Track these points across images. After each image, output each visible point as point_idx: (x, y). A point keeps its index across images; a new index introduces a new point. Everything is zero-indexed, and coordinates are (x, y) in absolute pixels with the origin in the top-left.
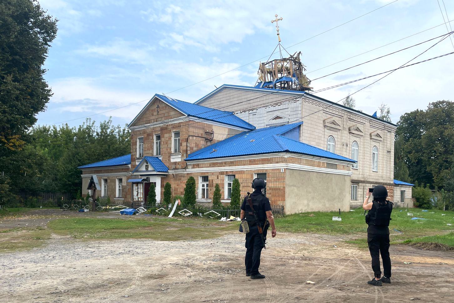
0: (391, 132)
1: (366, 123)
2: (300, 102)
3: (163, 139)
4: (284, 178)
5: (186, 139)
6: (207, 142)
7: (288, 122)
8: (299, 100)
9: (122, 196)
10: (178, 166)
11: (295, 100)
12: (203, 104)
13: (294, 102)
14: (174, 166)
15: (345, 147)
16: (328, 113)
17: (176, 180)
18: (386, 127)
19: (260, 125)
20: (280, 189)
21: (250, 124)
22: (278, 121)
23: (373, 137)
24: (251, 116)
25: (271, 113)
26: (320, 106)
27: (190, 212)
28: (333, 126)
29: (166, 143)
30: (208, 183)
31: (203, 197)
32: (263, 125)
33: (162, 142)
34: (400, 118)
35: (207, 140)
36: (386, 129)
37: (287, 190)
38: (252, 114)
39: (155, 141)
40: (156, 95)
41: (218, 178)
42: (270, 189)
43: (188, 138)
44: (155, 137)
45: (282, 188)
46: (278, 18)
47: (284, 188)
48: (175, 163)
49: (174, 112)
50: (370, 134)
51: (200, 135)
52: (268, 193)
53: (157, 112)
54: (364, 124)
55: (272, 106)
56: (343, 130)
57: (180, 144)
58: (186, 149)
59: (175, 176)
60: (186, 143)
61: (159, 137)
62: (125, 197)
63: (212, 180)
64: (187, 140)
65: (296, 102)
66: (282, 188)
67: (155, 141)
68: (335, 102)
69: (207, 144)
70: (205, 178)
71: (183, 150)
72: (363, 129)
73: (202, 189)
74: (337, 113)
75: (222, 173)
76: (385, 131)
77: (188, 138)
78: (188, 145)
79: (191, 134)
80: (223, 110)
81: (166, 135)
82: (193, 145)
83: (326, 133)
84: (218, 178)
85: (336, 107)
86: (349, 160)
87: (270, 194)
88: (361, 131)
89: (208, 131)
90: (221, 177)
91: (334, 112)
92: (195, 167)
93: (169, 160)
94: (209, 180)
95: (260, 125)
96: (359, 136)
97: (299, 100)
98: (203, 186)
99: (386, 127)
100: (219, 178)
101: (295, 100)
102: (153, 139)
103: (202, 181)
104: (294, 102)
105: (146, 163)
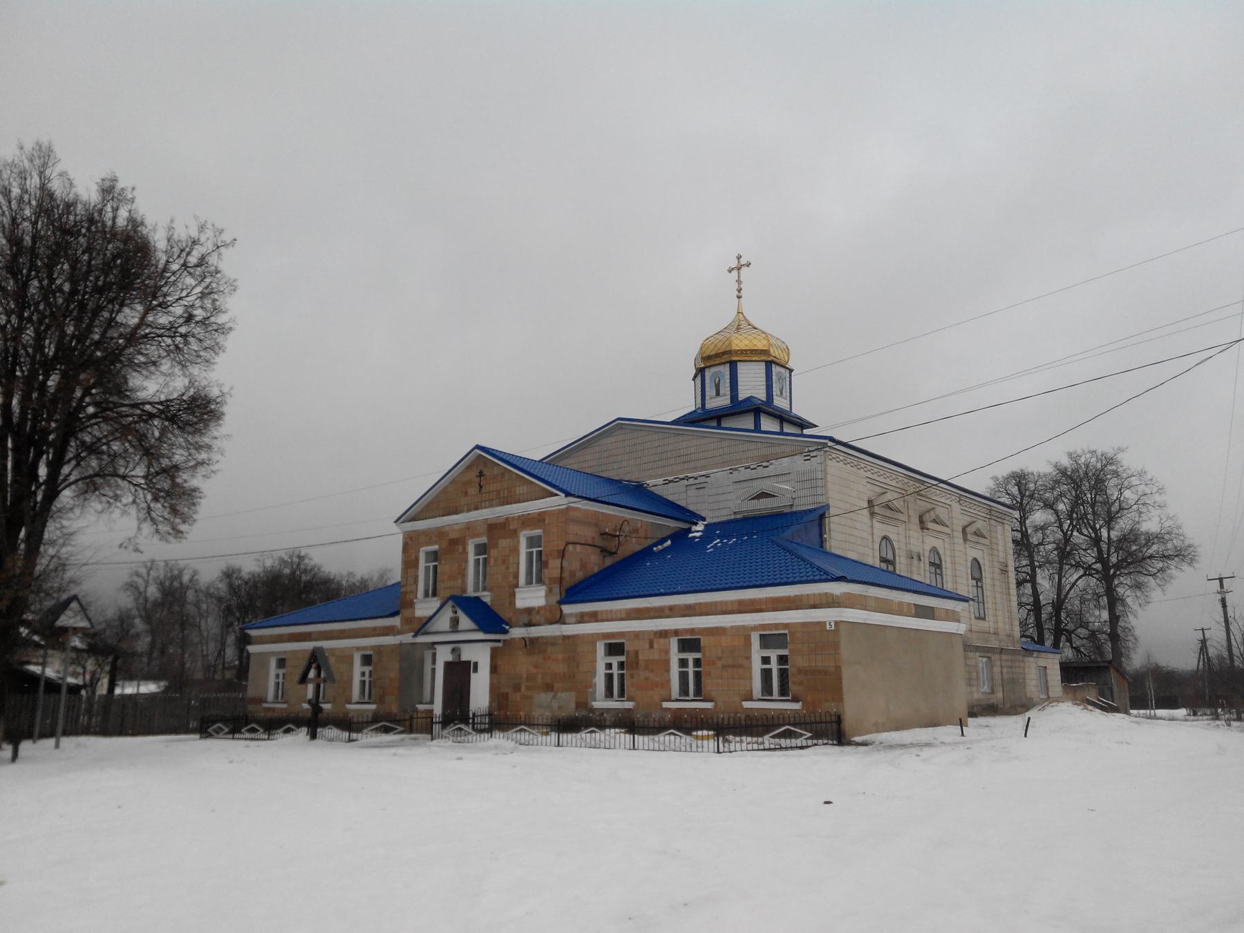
0: (1003, 523)
1: (953, 504)
2: (818, 460)
3: (494, 553)
4: (836, 645)
5: (558, 551)
6: (604, 557)
7: (792, 505)
8: (816, 456)
9: (370, 698)
10: (536, 618)
11: (805, 456)
12: (562, 464)
13: (805, 460)
14: (525, 619)
15: (915, 561)
16: (875, 482)
17: (530, 653)
18: (993, 513)
19: (716, 513)
20: (826, 672)
21: (690, 509)
22: (764, 505)
23: (970, 537)
24: (692, 492)
25: (743, 485)
26: (838, 460)
27: (805, 733)
28: (889, 513)
29: (504, 562)
30: (623, 658)
31: (609, 693)
32: (724, 512)
33: (492, 561)
34: (103, 180)
35: (605, 551)
36: (993, 517)
37: (846, 674)
38: (694, 487)
39: (471, 557)
40: (478, 447)
41: (651, 646)
42: (800, 671)
43: (564, 550)
44: (471, 549)
45: (832, 669)
46: (743, 261)
47: (838, 669)
48: (529, 611)
49: (525, 487)
50: (920, 516)
51: (590, 542)
52: (794, 683)
53: (478, 488)
54: (948, 507)
55: (746, 469)
56: (909, 522)
57: (543, 564)
58: (559, 576)
59: (527, 643)
60: (561, 560)
61: (481, 549)
62: (381, 701)
63: (637, 653)
64: (562, 554)
65: (809, 460)
66: (832, 669)
67: (471, 557)
68: (945, 479)
69: (604, 562)
70: (614, 649)
71: (550, 579)
72: (947, 513)
73: (606, 674)
74: (893, 483)
75: (664, 634)
76: (993, 522)
77: (564, 550)
78: (565, 564)
79: (571, 539)
80: (575, 467)
81: (504, 543)
82: (576, 565)
83: (876, 531)
84: (651, 646)
85: (873, 463)
86: (957, 596)
87: (801, 683)
88: (944, 524)
89: (607, 530)
90: (660, 642)
91: (887, 481)
92: (586, 619)
93: (512, 603)
94: (628, 652)
95: (716, 513)
96: (893, 522)
97: (816, 456)
98: (609, 666)
99: (993, 513)
100: (656, 646)
101: (805, 456)
102: (465, 552)
103: (606, 655)
104: (805, 460)
105: (453, 612)
